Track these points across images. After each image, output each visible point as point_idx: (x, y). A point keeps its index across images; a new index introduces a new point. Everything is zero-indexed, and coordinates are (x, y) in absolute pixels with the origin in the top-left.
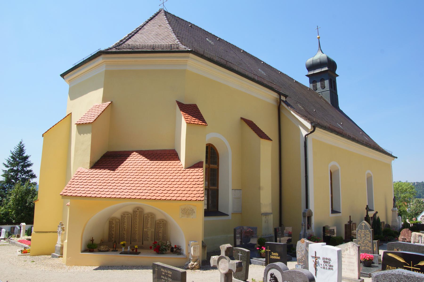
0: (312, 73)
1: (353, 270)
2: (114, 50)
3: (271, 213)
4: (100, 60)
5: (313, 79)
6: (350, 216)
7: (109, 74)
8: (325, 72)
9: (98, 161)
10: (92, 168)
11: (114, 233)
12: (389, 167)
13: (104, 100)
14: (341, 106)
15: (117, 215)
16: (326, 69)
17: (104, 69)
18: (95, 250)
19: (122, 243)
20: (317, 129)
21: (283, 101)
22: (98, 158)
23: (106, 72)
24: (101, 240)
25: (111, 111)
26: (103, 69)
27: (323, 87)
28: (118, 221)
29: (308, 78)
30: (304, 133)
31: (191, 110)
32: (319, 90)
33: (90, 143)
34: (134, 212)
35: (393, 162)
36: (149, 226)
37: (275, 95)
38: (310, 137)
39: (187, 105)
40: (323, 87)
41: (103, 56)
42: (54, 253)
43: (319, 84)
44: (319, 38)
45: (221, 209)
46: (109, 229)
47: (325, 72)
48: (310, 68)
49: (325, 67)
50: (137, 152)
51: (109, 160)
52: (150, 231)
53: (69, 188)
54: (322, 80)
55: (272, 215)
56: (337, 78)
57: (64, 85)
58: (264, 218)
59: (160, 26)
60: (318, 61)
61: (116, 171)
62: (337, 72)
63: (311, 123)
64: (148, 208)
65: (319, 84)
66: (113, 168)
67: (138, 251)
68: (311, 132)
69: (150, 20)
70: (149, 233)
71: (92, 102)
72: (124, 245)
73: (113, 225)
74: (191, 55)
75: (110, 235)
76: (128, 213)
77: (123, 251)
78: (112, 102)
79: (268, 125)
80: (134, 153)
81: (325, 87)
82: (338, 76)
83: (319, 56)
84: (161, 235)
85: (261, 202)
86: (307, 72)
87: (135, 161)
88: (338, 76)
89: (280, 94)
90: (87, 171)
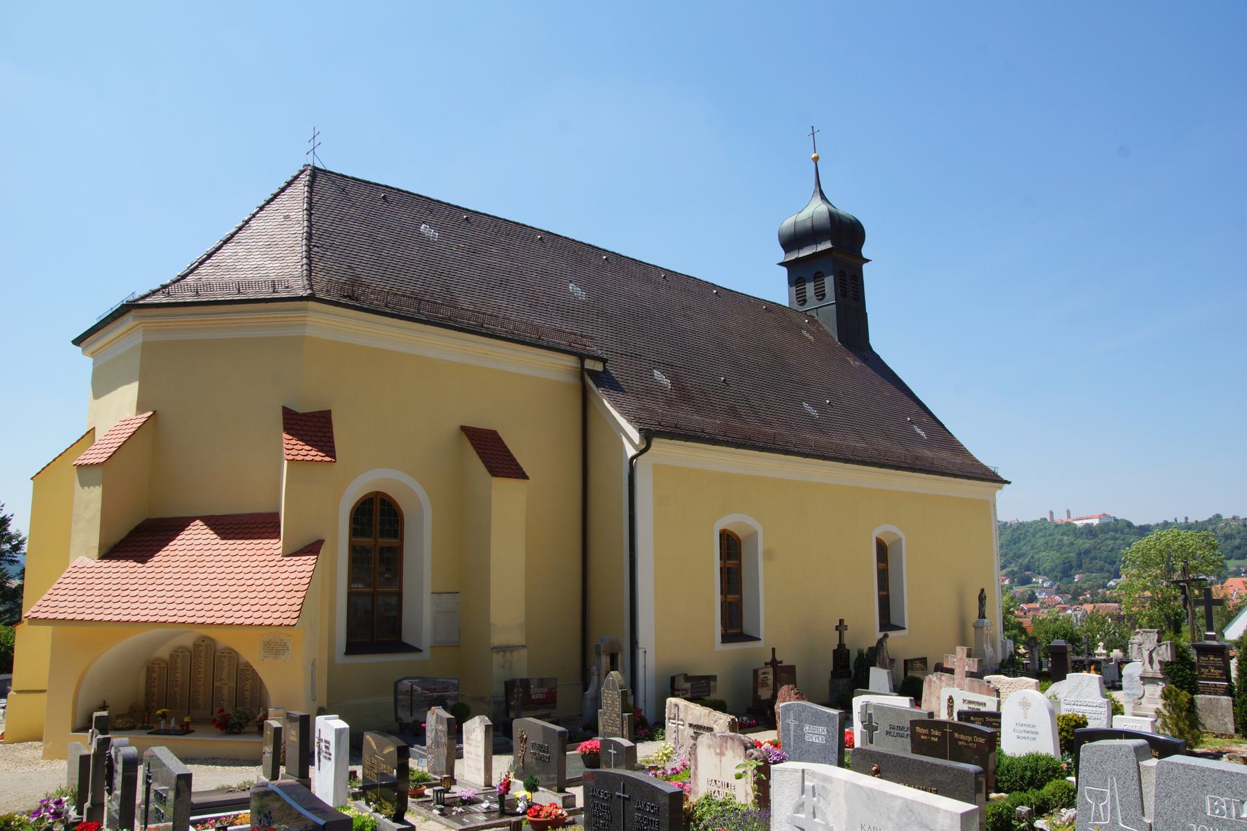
0: (793, 256)
1: (479, 770)
2: (159, 299)
3: (524, 646)
4: (129, 321)
5: (798, 273)
6: (774, 650)
7: (149, 350)
8: (830, 254)
9: (122, 541)
10: (103, 557)
11: (155, 690)
12: (989, 506)
13: (140, 408)
14: (879, 341)
15: (164, 652)
16: (827, 245)
17: (140, 340)
18: (247, 729)
19: (159, 712)
20: (656, 443)
21: (593, 374)
22: (120, 533)
23: (145, 346)
24: (131, 707)
25: (150, 436)
26: (137, 339)
27: (821, 295)
28: (163, 665)
29: (784, 270)
30: (631, 452)
31: (313, 428)
32: (812, 302)
33: (99, 506)
34: (196, 646)
35: (998, 493)
36: (224, 677)
37: (570, 362)
38: (641, 463)
39: (305, 414)
40: (821, 295)
41: (134, 312)
42: (561, 733)
43: (810, 288)
44: (816, 159)
45: (407, 638)
46: (147, 682)
47: (830, 254)
48: (791, 241)
49: (825, 240)
50: (202, 519)
51: (137, 539)
52: (227, 685)
53: (46, 604)
54: (818, 277)
55: (524, 651)
56: (865, 267)
57: (83, 364)
58: (497, 659)
59: (287, 217)
60: (809, 224)
61: (148, 564)
62: (865, 252)
63: (640, 430)
64: (224, 640)
65: (810, 288)
66: (143, 558)
67: (191, 728)
68: (642, 452)
69: (268, 202)
70: (225, 692)
71: (121, 411)
72: (164, 716)
73: (155, 675)
74: (311, 304)
75: (149, 693)
76: (182, 649)
77: (162, 727)
78: (155, 412)
79: (537, 441)
80: (198, 522)
81: (824, 295)
82: (867, 261)
83: (815, 210)
84: (247, 694)
85: (492, 620)
86: (781, 255)
87: (197, 537)
88: (867, 261)
89: (582, 357)
90: (92, 563)
